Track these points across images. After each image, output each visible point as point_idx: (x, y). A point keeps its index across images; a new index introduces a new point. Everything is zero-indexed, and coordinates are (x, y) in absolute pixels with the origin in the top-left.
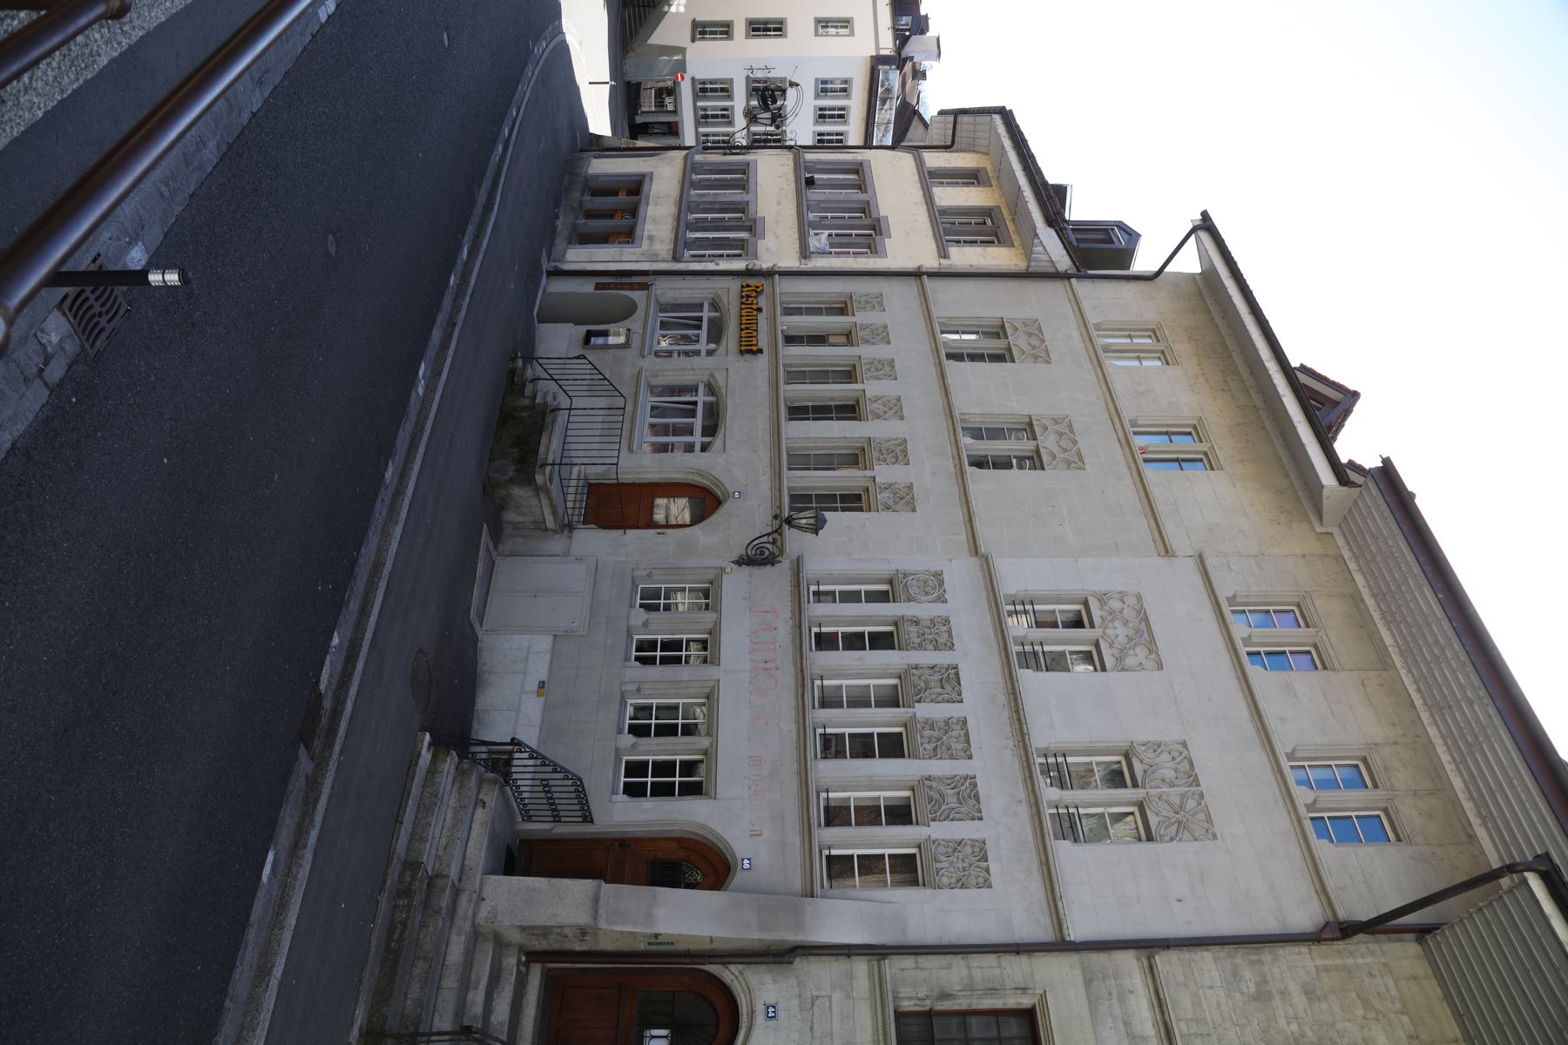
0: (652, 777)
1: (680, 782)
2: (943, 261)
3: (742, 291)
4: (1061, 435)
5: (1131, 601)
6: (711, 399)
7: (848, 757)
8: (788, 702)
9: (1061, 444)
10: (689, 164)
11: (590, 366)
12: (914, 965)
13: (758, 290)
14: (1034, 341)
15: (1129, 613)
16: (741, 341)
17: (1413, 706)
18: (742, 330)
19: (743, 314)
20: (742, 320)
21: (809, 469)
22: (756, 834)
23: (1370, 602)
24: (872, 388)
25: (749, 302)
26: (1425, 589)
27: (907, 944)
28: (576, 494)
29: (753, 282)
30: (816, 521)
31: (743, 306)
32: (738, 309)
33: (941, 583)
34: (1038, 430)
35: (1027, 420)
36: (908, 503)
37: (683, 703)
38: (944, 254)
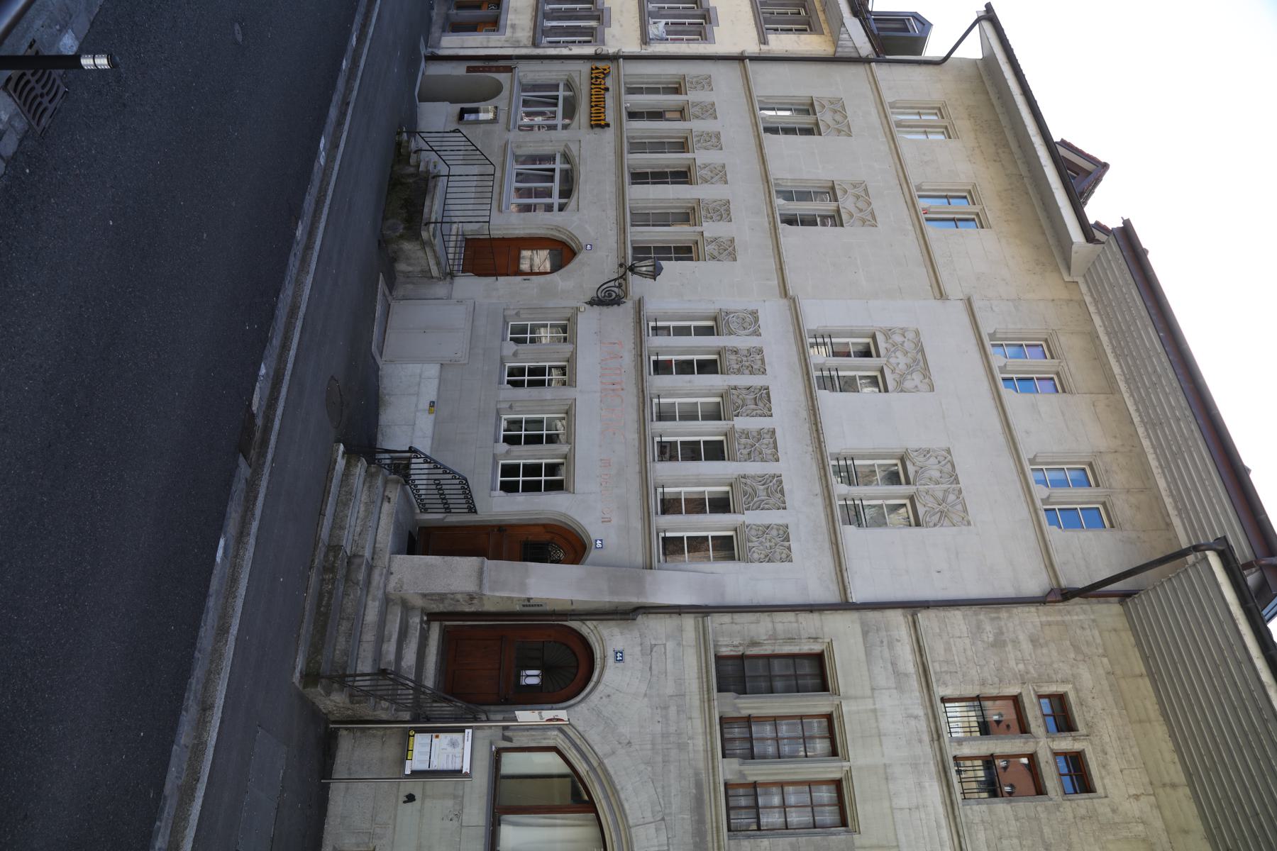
3: (592, 73)
5: (911, 335)
6: (566, 166)
8: (631, 416)
13: (605, 72)
14: (838, 117)
15: (909, 346)
16: (591, 117)
17: (1132, 422)
18: (592, 107)
19: (593, 93)
22: (606, 521)
23: (1104, 339)
25: (598, 83)
29: (601, 65)
30: (654, 269)
31: (593, 86)
33: (756, 320)
34: (839, 193)
35: (830, 184)
38: (763, 41)
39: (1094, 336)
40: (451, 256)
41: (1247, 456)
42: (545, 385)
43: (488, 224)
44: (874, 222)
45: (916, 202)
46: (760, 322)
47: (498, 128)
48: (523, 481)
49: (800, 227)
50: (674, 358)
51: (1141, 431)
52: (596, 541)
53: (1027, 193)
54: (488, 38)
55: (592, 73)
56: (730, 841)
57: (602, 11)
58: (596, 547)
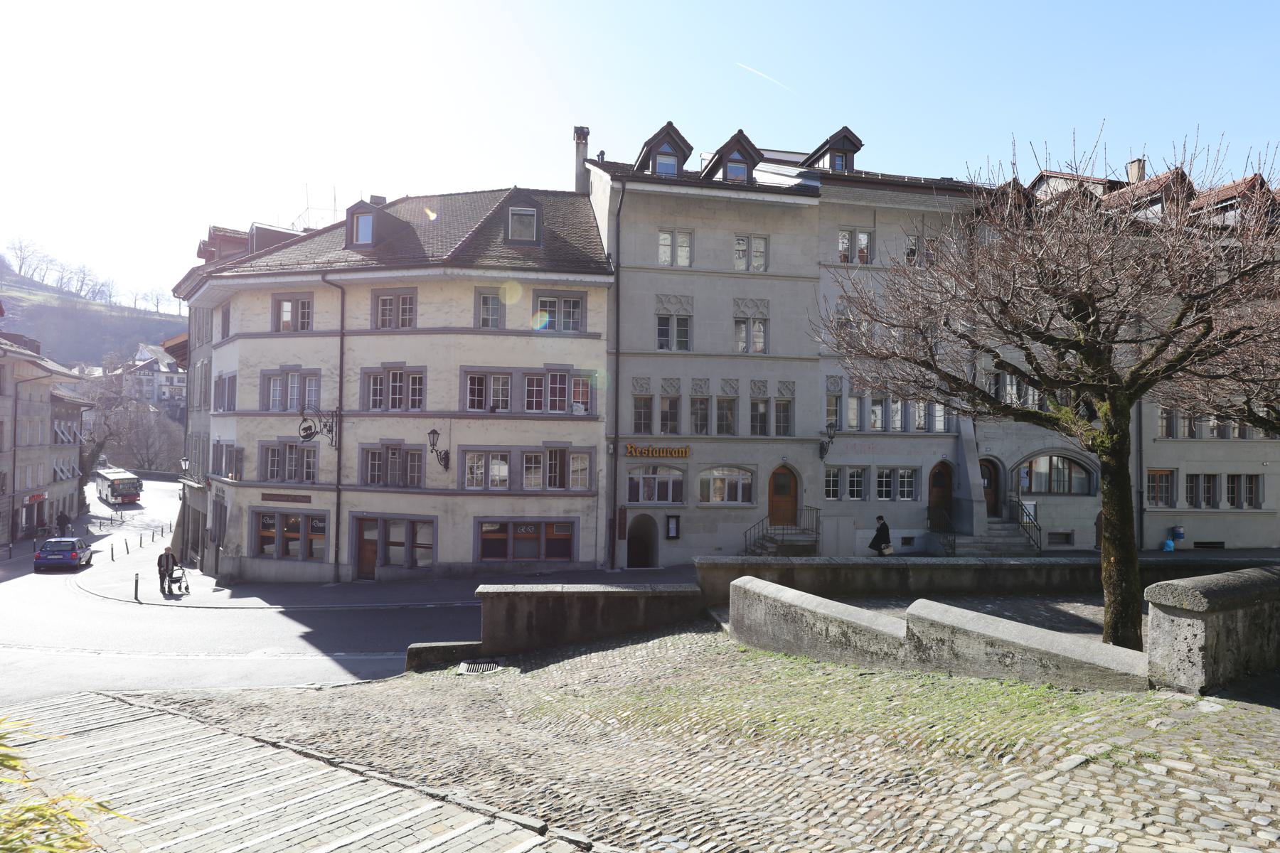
2: (602, 338)
7: (1201, 479)
8: (886, 440)
10: (363, 488)
11: (753, 529)
17: (892, 208)
18: (653, 456)
21: (1149, 482)
22: (935, 453)
23: (845, 202)
24: (715, 391)
29: (621, 450)
30: (876, 435)
33: (832, 377)
36: (485, 322)
38: (596, 336)
40: (794, 532)
41: (936, 175)
47: (682, 514)
51: (897, 206)
54: (583, 528)
55: (636, 456)
56: (421, 323)
57: (382, 445)
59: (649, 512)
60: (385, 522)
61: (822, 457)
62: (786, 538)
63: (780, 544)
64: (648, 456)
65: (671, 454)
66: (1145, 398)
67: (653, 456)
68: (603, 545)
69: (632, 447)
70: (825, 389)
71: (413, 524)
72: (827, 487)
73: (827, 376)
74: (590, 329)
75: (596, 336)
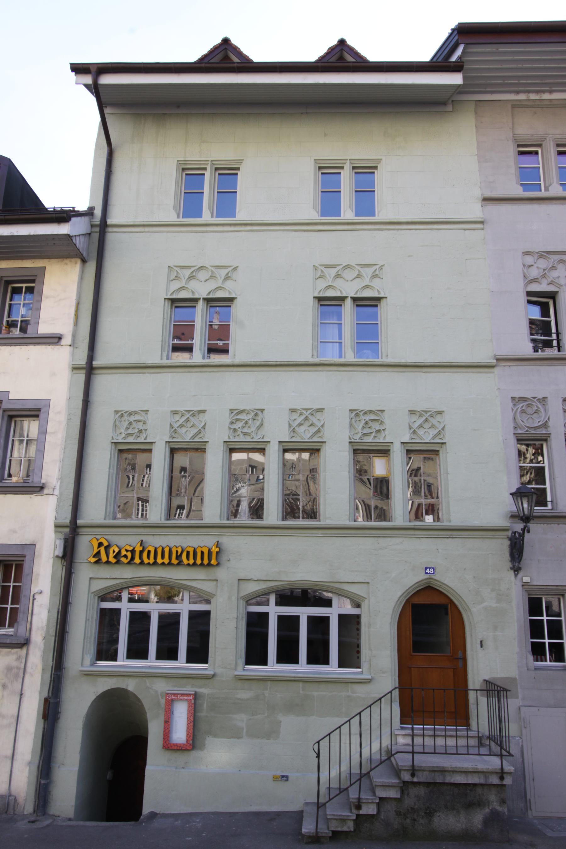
0: (544, 638)
1: (543, 620)
2: (63, 342)
3: (108, 562)
4: (338, 276)
5: (529, 260)
6: (272, 599)
9: (203, 280)
12: (35, 442)
13: (106, 544)
14: (202, 275)
15: (543, 264)
16: (202, 564)
18: (142, 563)
19: (191, 561)
20: (163, 564)
25: (129, 555)
26: (501, 50)
27: (84, 446)
28: (424, 735)
31: (137, 560)
32: (107, 567)
34: (330, 293)
35: (168, 304)
37: (561, 621)
38: (56, 339)
39: (516, 106)
42: (5, 626)
43: (435, 690)
44: (377, 267)
45: (239, 222)
46: (528, 395)
48: (549, 639)
49: (230, 342)
50: (548, 486)
52: (426, 573)
53: (411, 112)
55: (108, 562)
58: (434, 573)
59: (131, 685)
60: (542, 661)
61: (516, 570)
62: (422, 760)
63: (406, 777)
64: (131, 562)
65: (178, 557)
66: (483, 742)
67: (142, 563)
68: (28, 757)
69: (100, 544)
70: (512, 425)
71: (537, 661)
72: (4, 581)
73: (513, 399)
74: (44, 329)
75: (56, 339)
